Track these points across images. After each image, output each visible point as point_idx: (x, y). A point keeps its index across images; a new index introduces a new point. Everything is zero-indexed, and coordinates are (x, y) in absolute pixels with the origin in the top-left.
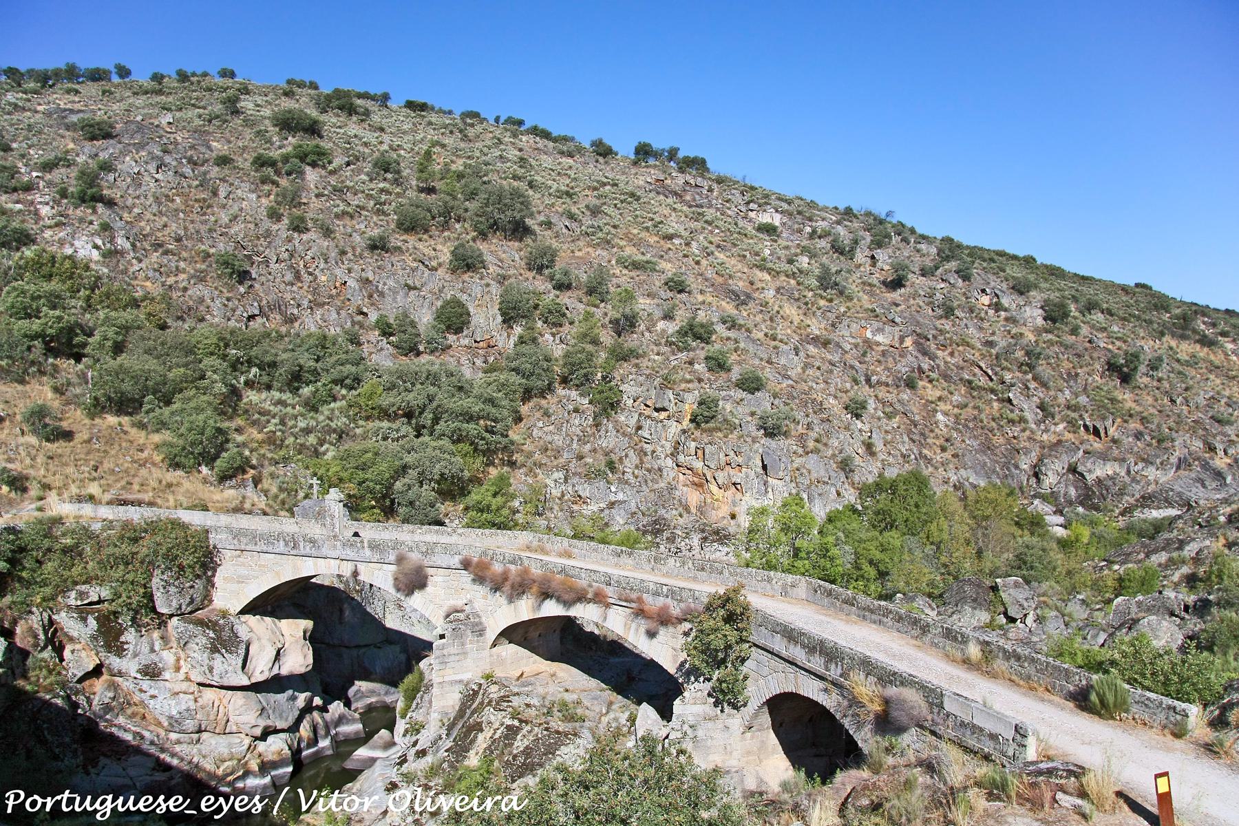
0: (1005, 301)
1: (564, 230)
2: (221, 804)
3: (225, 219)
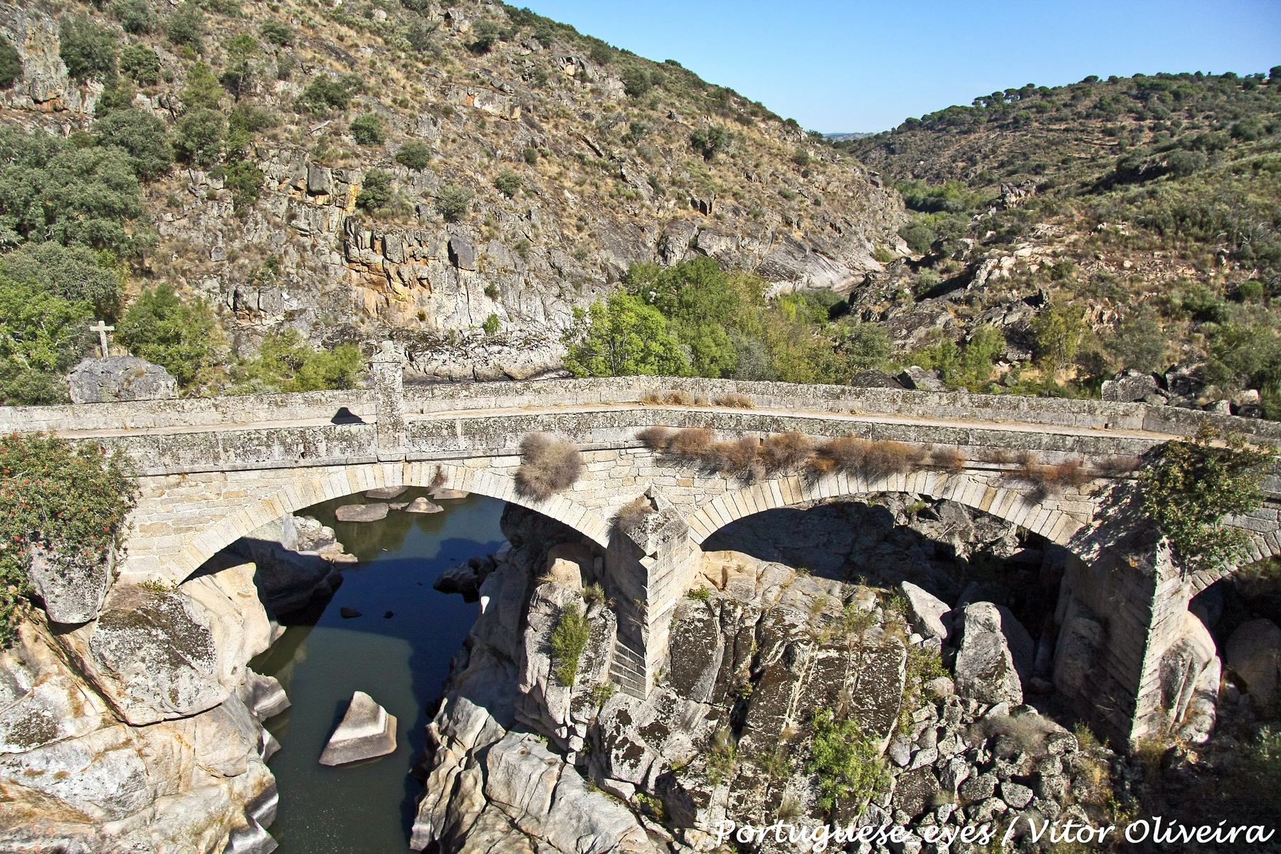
0: (590, 71)
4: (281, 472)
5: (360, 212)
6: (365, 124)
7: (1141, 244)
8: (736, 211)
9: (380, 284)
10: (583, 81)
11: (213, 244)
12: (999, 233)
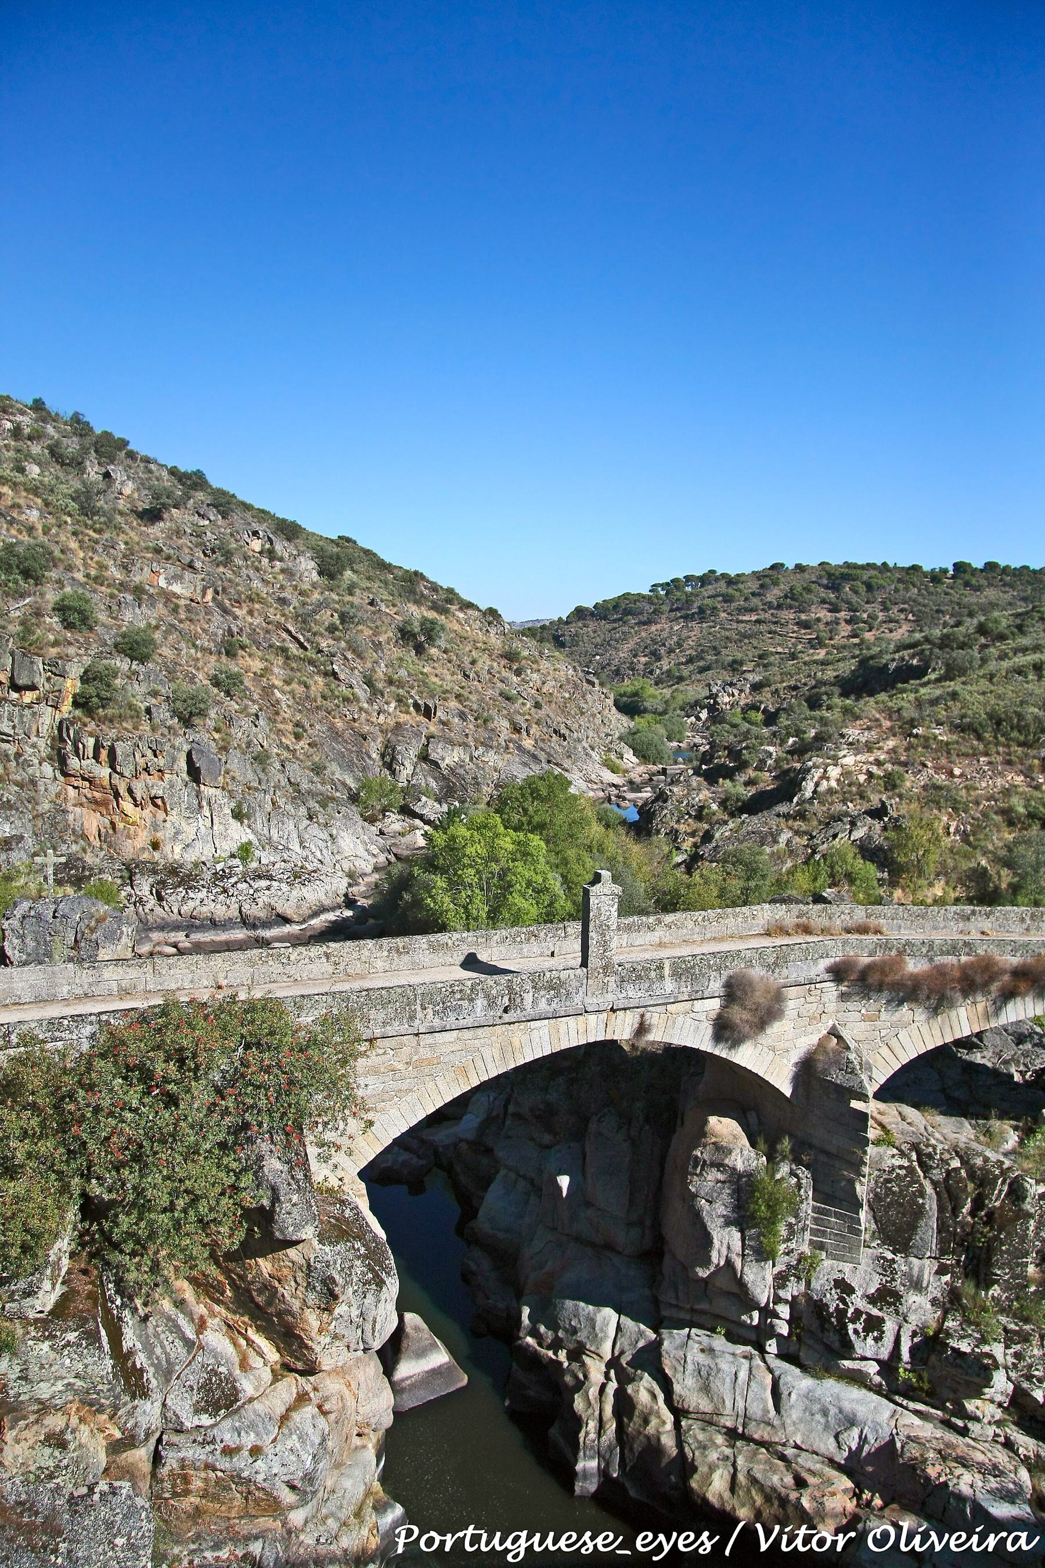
0: (278, 547)
2: (661, 1542)
4: (481, 1030)
5: (78, 713)
6: (76, 604)
7: (964, 749)
8: (462, 716)
9: (104, 803)
10: (271, 560)
12: (802, 740)
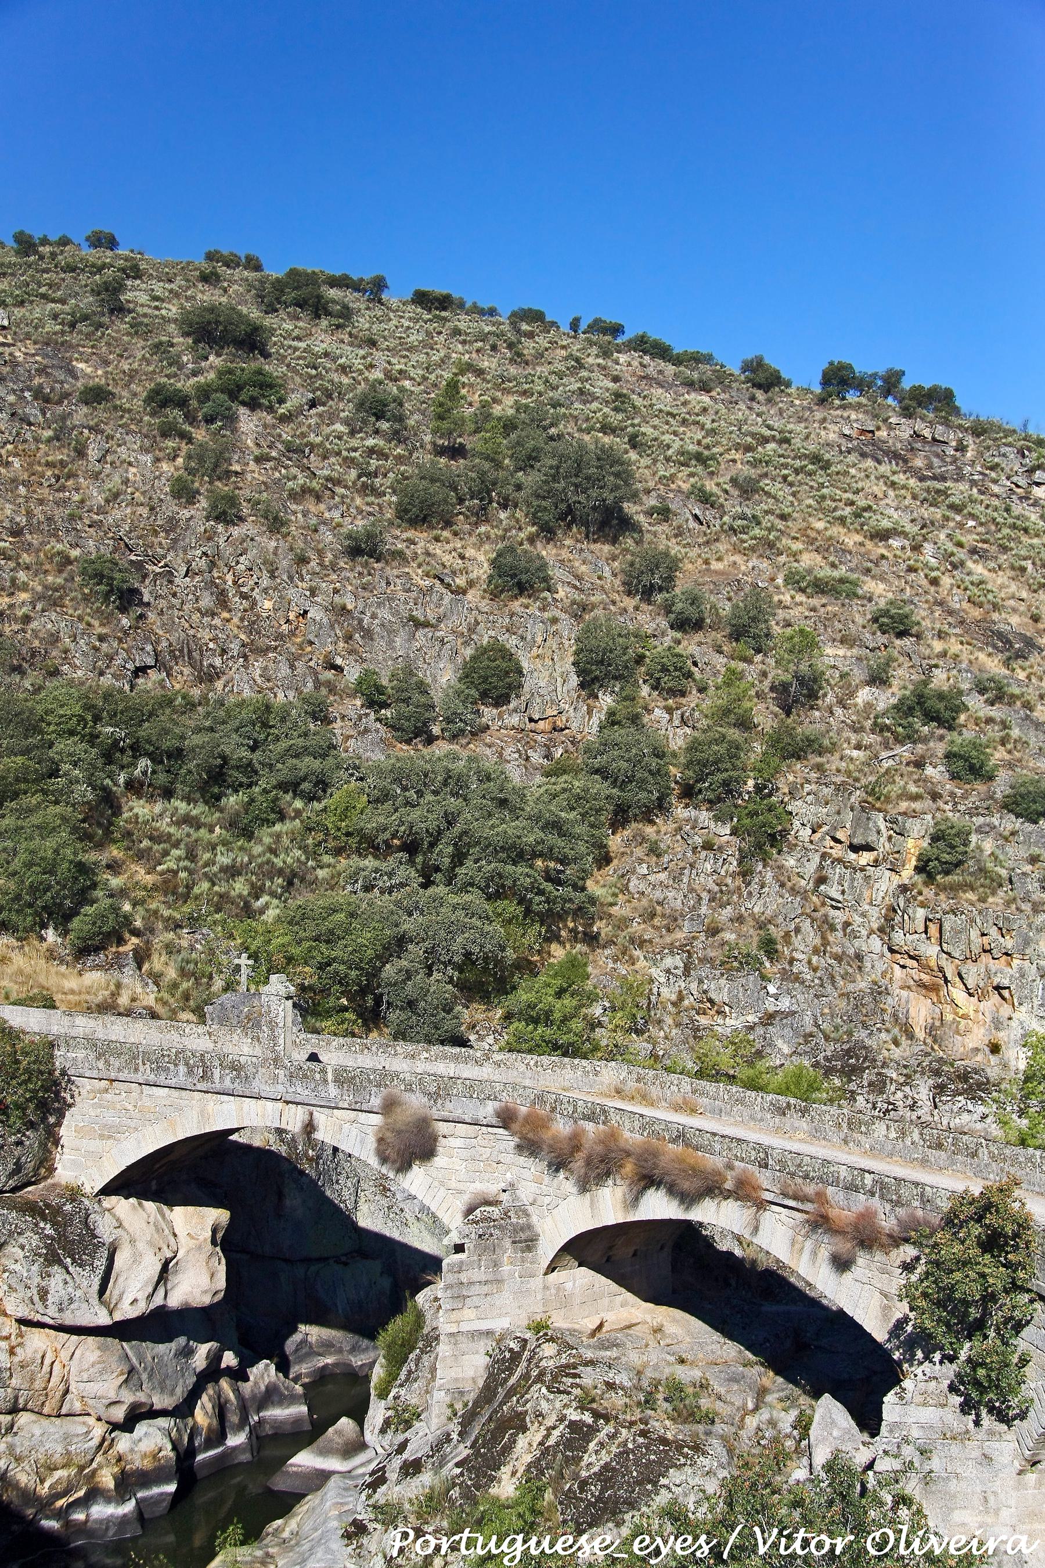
1: (692, 524)
3: (98, 499)
4: (184, 1093)
9: (933, 988)
11: (693, 908)
